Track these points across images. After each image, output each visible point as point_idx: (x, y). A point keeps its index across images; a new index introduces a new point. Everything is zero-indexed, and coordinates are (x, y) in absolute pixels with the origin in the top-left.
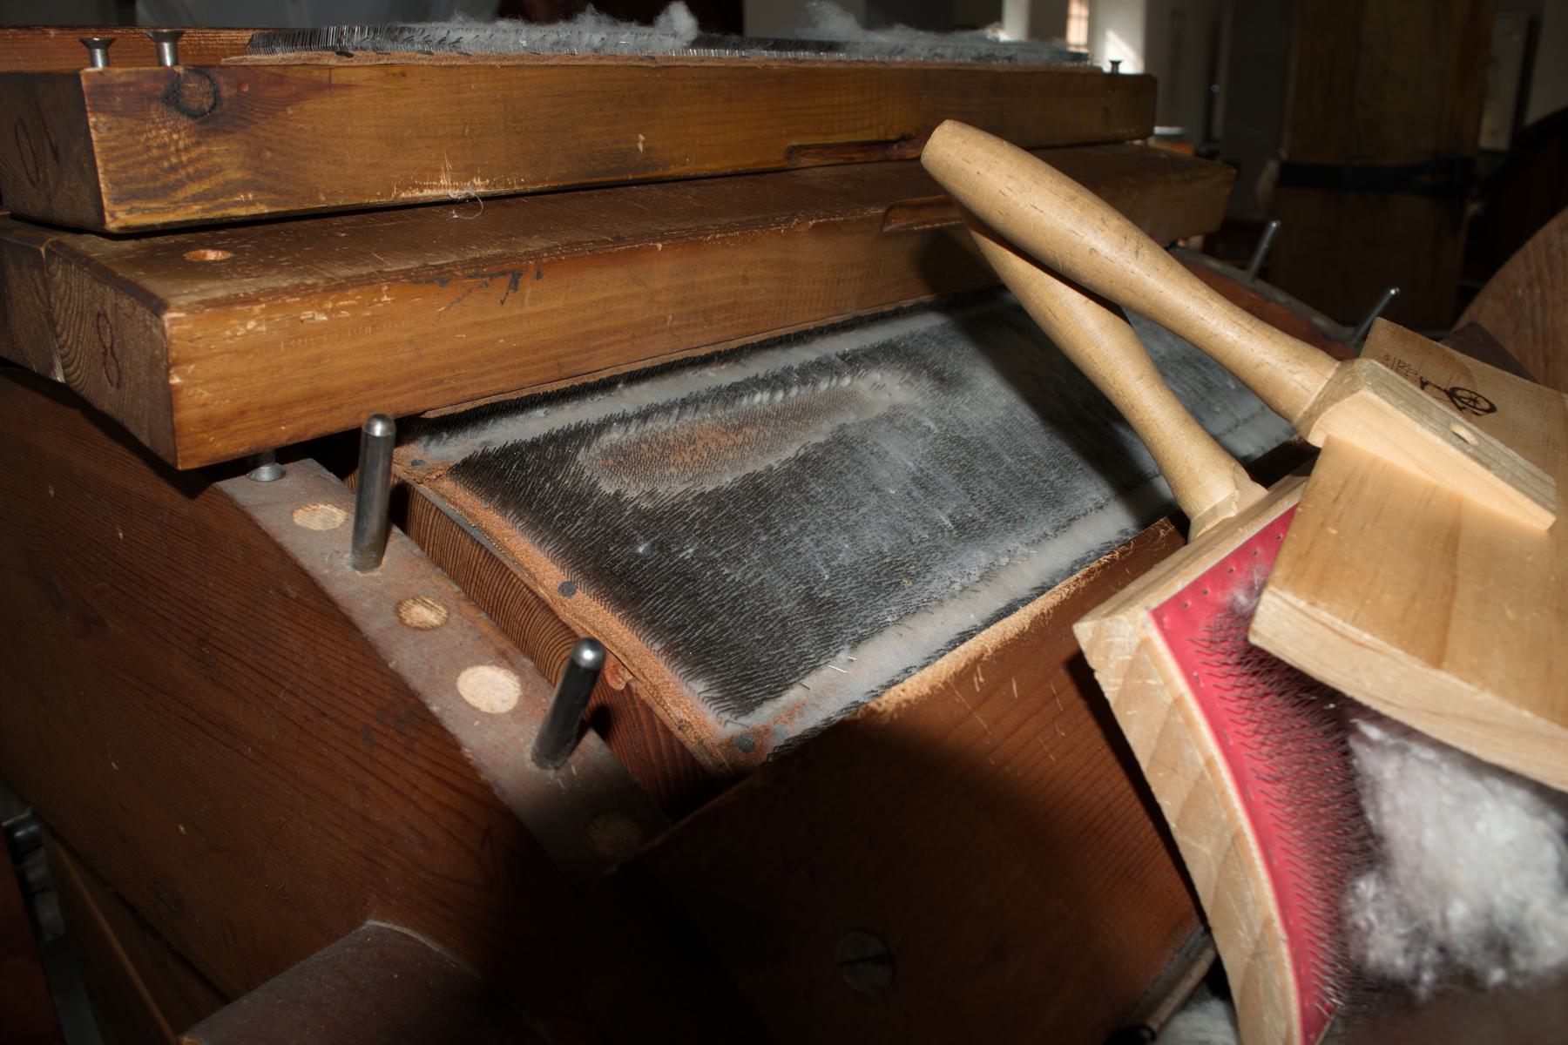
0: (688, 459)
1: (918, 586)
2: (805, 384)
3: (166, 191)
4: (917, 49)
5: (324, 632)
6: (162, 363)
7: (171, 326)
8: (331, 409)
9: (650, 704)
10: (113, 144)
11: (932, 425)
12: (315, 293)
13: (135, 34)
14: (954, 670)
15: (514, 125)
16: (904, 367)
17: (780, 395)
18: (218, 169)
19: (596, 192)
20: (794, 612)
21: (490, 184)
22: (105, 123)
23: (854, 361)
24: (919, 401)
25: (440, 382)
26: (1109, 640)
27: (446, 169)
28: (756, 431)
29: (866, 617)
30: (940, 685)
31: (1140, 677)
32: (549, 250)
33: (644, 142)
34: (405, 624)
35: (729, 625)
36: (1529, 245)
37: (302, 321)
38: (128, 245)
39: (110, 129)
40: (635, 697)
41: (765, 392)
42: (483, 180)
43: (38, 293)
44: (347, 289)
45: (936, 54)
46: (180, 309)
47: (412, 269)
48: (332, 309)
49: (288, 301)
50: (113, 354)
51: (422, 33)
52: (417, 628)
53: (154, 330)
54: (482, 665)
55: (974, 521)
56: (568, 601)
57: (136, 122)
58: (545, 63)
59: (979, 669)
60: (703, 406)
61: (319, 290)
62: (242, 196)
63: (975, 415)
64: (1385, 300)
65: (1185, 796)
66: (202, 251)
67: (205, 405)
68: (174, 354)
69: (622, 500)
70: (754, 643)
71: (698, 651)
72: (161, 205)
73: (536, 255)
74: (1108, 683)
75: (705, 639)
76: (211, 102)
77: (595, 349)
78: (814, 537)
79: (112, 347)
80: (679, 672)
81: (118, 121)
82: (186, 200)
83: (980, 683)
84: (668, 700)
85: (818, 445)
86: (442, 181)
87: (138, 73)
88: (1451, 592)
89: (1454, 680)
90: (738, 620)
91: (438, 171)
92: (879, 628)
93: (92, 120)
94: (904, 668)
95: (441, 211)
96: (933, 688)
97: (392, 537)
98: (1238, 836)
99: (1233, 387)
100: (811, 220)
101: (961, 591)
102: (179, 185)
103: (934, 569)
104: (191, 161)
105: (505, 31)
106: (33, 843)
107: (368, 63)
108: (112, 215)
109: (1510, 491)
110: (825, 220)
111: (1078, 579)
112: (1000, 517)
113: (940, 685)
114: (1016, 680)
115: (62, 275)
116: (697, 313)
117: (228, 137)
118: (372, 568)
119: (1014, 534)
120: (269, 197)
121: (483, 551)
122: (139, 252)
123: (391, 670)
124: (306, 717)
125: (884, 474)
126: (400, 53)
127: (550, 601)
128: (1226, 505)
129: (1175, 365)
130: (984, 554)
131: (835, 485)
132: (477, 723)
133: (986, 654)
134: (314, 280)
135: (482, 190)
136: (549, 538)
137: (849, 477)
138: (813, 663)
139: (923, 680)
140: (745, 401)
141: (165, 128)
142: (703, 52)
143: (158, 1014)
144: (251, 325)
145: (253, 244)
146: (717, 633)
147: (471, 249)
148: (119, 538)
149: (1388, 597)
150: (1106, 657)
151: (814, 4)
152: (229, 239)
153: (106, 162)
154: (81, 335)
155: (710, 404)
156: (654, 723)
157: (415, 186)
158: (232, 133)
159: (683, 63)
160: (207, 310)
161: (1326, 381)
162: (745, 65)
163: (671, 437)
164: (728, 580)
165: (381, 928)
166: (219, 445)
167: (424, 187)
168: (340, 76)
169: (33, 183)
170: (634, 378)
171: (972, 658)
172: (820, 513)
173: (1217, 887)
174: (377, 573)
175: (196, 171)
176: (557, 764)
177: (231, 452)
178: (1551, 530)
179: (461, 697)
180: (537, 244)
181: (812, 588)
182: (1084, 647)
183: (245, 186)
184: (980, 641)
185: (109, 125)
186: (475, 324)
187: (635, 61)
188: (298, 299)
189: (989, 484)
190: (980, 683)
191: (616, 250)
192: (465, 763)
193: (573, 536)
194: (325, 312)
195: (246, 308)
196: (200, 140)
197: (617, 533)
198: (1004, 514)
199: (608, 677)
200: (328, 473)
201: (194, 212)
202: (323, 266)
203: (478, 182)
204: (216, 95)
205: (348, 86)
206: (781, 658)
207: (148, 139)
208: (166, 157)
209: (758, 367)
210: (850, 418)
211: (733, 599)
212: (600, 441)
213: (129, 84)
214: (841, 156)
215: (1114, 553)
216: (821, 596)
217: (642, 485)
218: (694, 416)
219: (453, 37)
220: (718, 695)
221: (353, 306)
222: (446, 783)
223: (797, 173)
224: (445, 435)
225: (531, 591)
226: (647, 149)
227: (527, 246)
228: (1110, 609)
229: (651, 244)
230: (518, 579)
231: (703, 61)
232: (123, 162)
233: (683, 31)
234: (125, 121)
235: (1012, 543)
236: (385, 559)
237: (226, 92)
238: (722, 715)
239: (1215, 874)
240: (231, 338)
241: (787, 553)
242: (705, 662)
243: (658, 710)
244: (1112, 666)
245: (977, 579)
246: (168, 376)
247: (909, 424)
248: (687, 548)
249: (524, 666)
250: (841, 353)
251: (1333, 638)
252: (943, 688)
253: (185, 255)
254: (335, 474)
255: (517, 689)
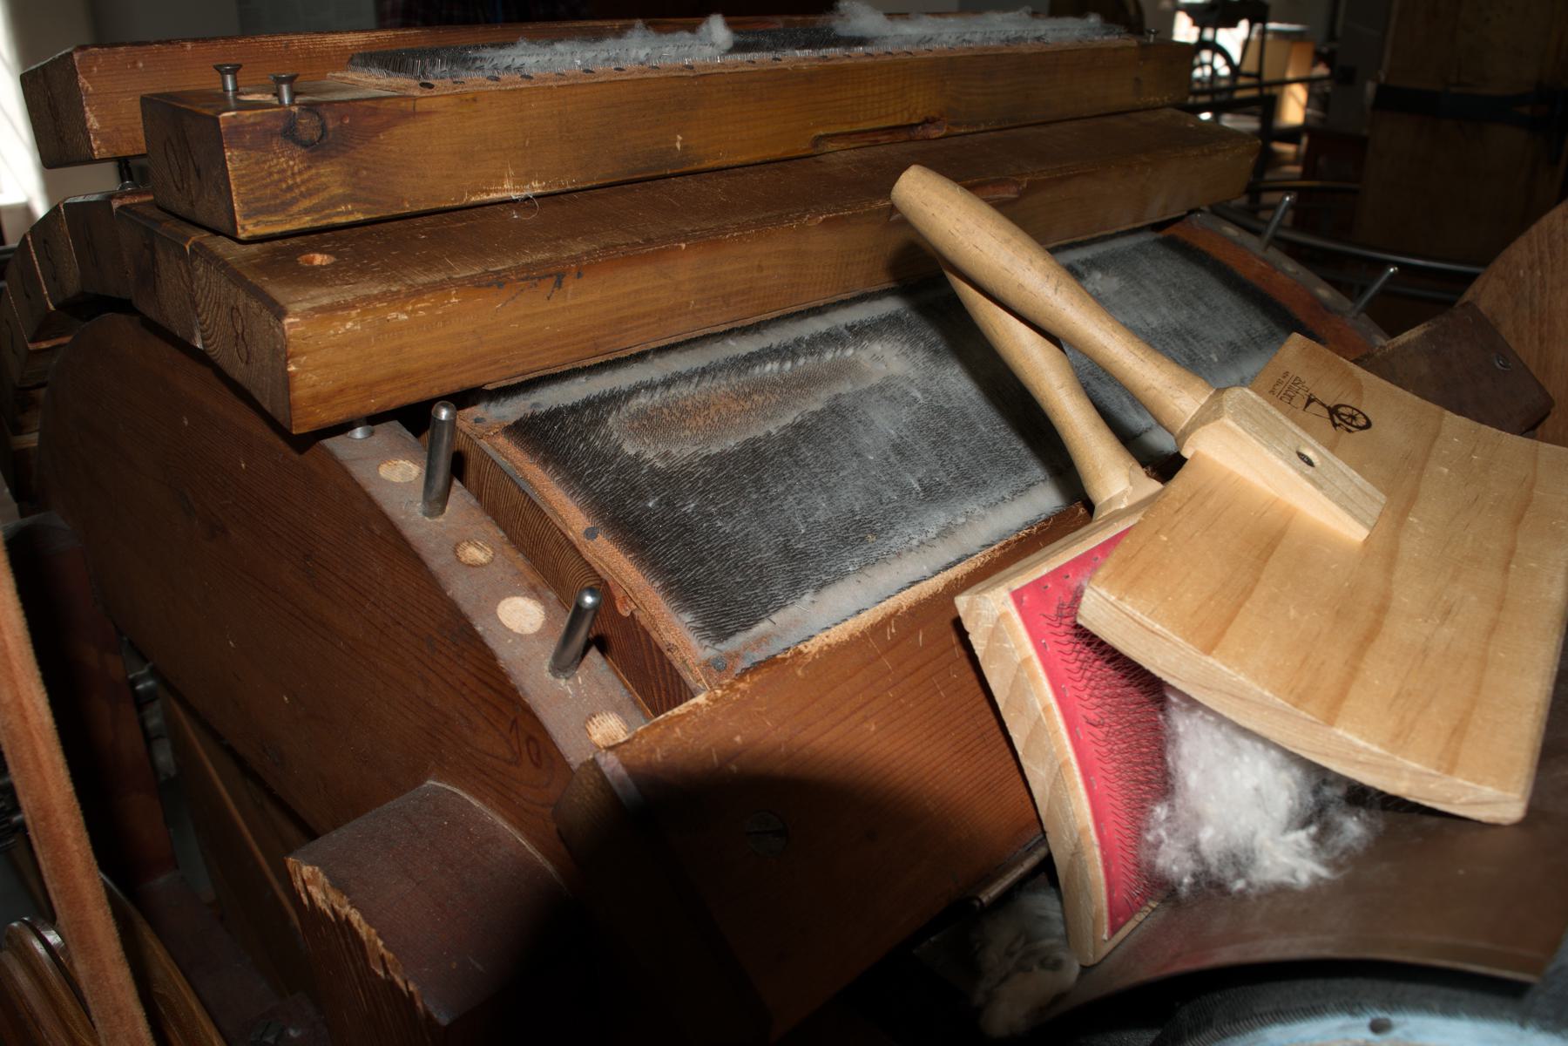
0: (701, 423)
1: (880, 541)
2: (812, 354)
3: (284, 206)
4: (945, 37)
5: (400, 563)
6: (282, 355)
7: (289, 328)
8: (410, 385)
9: (648, 629)
10: (244, 172)
11: (919, 395)
12: (399, 298)
13: (256, 42)
14: (871, 622)
15: (567, 134)
16: (903, 340)
17: (788, 365)
18: (324, 187)
19: (638, 185)
20: (771, 560)
21: (546, 186)
22: (237, 156)
23: (860, 332)
24: (912, 373)
25: (496, 362)
26: (978, 611)
27: (509, 176)
28: (763, 398)
29: (831, 566)
30: (858, 634)
31: (998, 642)
32: (588, 253)
33: (681, 142)
34: (461, 562)
35: (717, 569)
36: (1534, 229)
37: (388, 321)
38: (254, 248)
39: (241, 161)
40: (637, 623)
41: (775, 363)
42: (540, 182)
43: (182, 279)
44: (424, 294)
45: (964, 40)
46: (296, 315)
47: (476, 275)
48: (412, 311)
49: (378, 306)
50: (243, 339)
51: (491, 62)
52: (469, 565)
53: (276, 330)
54: (517, 596)
55: (940, 485)
56: (591, 544)
57: (261, 153)
58: (595, 80)
59: (893, 622)
60: (720, 375)
61: (402, 296)
62: (343, 208)
63: (960, 386)
64: (1385, 277)
65: (1028, 732)
66: (312, 255)
67: (314, 386)
68: (291, 350)
69: (640, 461)
70: (735, 585)
71: (688, 590)
72: (280, 218)
73: (577, 259)
74: (977, 643)
75: (695, 580)
76: (319, 133)
77: (627, 330)
78: (797, 496)
79: (242, 334)
80: (673, 605)
81: (247, 154)
82: (299, 213)
83: (891, 634)
84: (662, 627)
85: (814, 413)
86: (505, 186)
87: (263, 114)
88: (1247, 592)
89: (1218, 665)
90: (724, 565)
91: (502, 177)
92: (841, 575)
93: (228, 154)
94: (857, 609)
95: (505, 209)
96: (851, 636)
97: (453, 489)
98: (1066, 763)
99: (1216, 360)
100: (822, 215)
101: (918, 546)
102: (295, 201)
103: (897, 527)
104: (303, 182)
105: (562, 54)
106: (151, 696)
107: (446, 93)
108: (243, 228)
109: (1334, 507)
110: (834, 214)
111: (994, 550)
112: (965, 481)
113: (858, 634)
114: (923, 631)
115: (204, 271)
116: (716, 297)
117: (332, 161)
118: (437, 516)
119: (974, 496)
120: (365, 207)
121: (528, 498)
122: (263, 256)
123: (449, 598)
124: (385, 624)
125: (867, 440)
126: (474, 80)
127: (577, 542)
128: (1120, 497)
129: (1164, 337)
130: (944, 514)
131: (822, 450)
132: (510, 641)
133: (901, 611)
134: (398, 287)
135: (539, 191)
136: (579, 491)
137: (835, 443)
138: (781, 603)
139: (845, 629)
140: (757, 370)
141: (284, 157)
142: (739, 57)
143: (256, 849)
144: (349, 325)
145: (352, 247)
146: (705, 576)
147: (525, 254)
148: (241, 468)
149: (1190, 595)
150: (977, 624)
151: (846, 4)
152: (332, 242)
153: (238, 186)
154: (218, 319)
155: (725, 374)
156: (651, 644)
157: (482, 191)
158: (336, 157)
159: (719, 71)
160: (316, 316)
161: (1199, 406)
162: (776, 67)
163: (689, 403)
164: (721, 531)
165: (436, 787)
166: (323, 415)
167: (491, 191)
168: (422, 105)
169: (178, 190)
170: (661, 351)
171: (889, 613)
172: (806, 475)
173: (1049, 801)
174: (441, 519)
175: (308, 190)
176: (567, 675)
177: (332, 420)
178: (1366, 542)
179: (499, 620)
180: (579, 247)
181: (789, 540)
182: (961, 615)
183: (344, 199)
184: (900, 599)
185: (240, 158)
186: (526, 316)
187: (675, 71)
188: (385, 304)
189: (960, 451)
190: (891, 634)
191: (645, 251)
192: (499, 670)
193: (597, 490)
194: (406, 312)
195: (345, 313)
196: (311, 164)
197: (633, 489)
198: (969, 478)
199: (618, 606)
200: (408, 432)
201: (306, 222)
202: (405, 272)
203: (536, 184)
204: (323, 127)
205: (429, 113)
206: (756, 597)
207: (270, 167)
208: (284, 180)
209: (772, 338)
210: (845, 387)
211: (722, 547)
212: (629, 404)
213: (254, 124)
214: (867, 139)
215: (1033, 528)
216: (795, 547)
217: (660, 445)
218: (712, 382)
219: (518, 62)
220: (702, 625)
221: (428, 307)
222: (486, 683)
223: (822, 158)
224: (502, 400)
225: (562, 533)
226: (684, 148)
227: (572, 250)
228: (985, 586)
229: (676, 244)
230: (553, 523)
231: (737, 67)
232: (252, 186)
233: (720, 42)
234: (253, 153)
235: (971, 505)
236: (448, 508)
237: (331, 125)
238: (702, 641)
239: (1048, 793)
240: (334, 336)
241: (772, 509)
242: (692, 599)
243: (654, 635)
244: (980, 631)
245: (935, 536)
246: (287, 365)
247: (897, 395)
248: (689, 504)
249: (548, 598)
250: (849, 325)
251: (1134, 626)
252: (860, 636)
253: (299, 259)
254: (413, 433)
255: (542, 616)
